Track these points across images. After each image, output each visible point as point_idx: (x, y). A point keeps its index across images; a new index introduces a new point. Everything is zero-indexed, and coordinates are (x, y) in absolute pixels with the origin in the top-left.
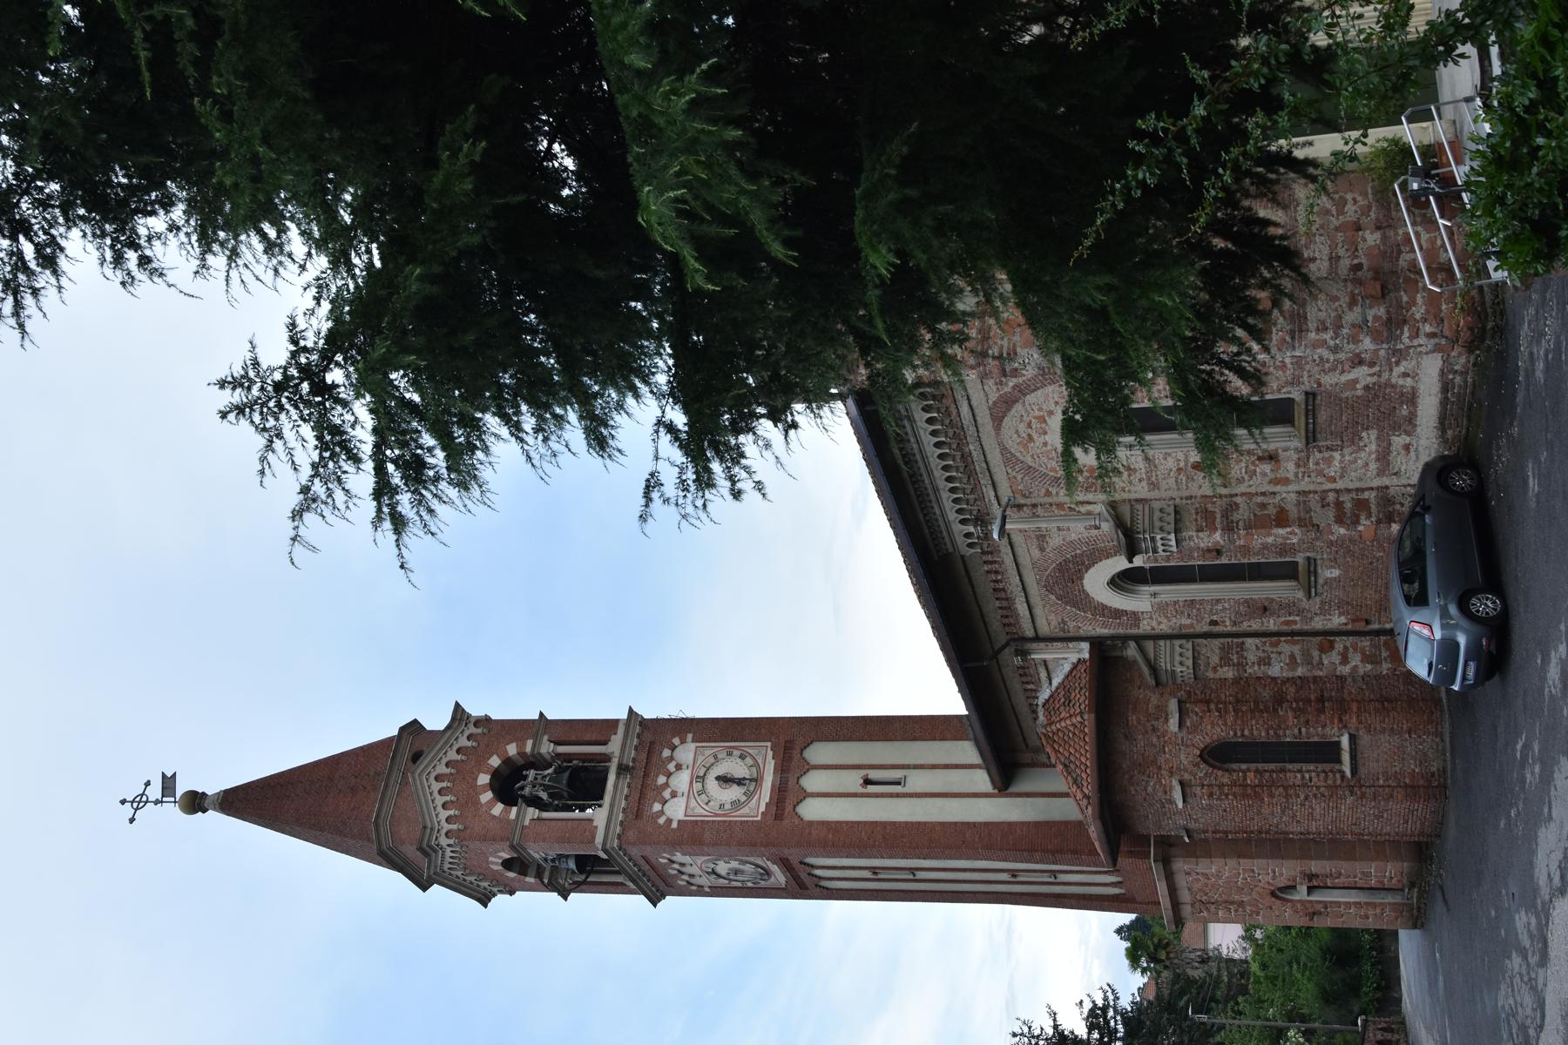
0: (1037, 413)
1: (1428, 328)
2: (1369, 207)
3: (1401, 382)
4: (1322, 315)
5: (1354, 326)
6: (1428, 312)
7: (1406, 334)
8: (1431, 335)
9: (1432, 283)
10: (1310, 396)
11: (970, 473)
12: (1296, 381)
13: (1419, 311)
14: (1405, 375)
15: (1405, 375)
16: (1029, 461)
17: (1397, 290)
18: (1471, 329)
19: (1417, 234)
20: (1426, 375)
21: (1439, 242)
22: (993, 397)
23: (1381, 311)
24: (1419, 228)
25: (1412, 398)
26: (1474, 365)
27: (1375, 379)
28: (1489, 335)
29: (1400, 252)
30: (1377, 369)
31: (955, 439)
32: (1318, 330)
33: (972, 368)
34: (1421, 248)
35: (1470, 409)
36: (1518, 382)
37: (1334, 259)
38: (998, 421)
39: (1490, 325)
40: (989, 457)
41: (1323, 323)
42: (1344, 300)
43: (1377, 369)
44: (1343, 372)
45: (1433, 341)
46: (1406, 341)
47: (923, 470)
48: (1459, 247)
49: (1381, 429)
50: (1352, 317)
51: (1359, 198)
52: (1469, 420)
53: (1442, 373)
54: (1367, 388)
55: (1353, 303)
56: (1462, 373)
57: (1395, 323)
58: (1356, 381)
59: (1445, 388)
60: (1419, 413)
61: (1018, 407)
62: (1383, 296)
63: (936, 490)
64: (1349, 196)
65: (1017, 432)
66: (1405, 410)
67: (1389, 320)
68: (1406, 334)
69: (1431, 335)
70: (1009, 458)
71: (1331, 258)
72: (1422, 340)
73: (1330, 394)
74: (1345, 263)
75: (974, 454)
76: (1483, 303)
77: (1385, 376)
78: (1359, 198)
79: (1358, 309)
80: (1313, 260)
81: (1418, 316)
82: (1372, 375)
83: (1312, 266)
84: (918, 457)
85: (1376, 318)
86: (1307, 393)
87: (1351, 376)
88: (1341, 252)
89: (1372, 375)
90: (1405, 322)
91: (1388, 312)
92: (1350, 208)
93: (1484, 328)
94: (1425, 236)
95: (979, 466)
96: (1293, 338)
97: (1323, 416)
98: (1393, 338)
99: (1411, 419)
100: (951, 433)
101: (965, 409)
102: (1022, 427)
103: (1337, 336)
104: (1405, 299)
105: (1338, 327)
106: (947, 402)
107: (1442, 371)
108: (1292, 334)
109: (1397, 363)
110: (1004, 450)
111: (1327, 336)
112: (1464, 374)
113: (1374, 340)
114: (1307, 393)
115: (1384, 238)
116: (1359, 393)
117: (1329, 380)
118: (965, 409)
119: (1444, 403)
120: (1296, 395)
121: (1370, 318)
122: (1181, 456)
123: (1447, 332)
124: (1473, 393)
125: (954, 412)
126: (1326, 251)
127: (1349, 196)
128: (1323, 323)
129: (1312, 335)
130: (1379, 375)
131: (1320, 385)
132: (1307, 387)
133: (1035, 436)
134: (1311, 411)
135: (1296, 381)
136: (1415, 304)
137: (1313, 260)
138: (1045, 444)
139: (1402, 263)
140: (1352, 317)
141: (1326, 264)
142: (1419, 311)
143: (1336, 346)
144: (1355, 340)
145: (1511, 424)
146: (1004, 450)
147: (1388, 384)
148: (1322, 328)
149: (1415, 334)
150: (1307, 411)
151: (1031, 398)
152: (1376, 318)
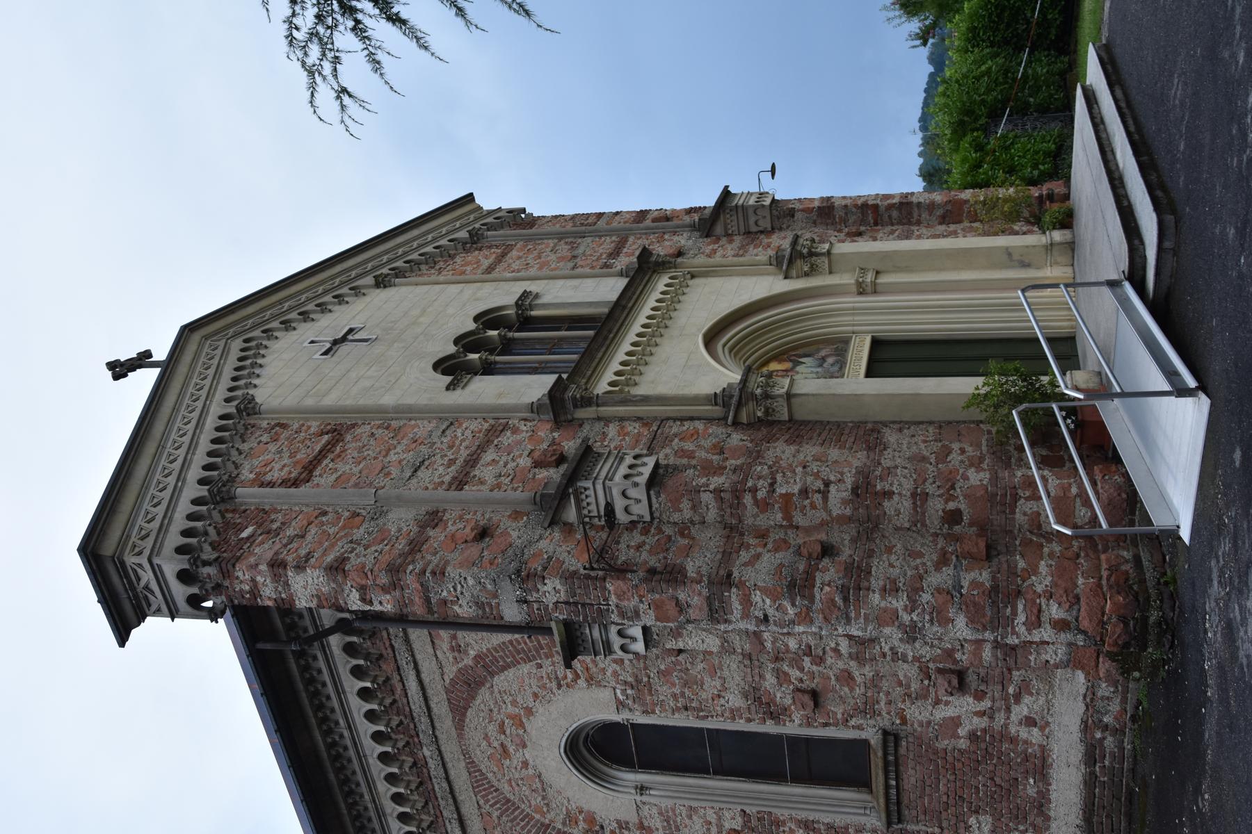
0: (511, 709)
1: (1055, 611)
2: (981, 459)
3: (1024, 733)
4: (896, 572)
5: (939, 590)
6: (1054, 584)
7: (1021, 618)
8: (1060, 625)
9: (1058, 522)
10: (890, 737)
11: (430, 798)
12: (867, 709)
13: (1042, 580)
14: (1030, 722)
15: (1030, 722)
16: (506, 788)
17: (1010, 551)
18: (1123, 620)
19: (1043, 478)
20: (1062, 716)
21: (1074, 490)
22: (451, 671)
23: (985, 577)
24: (1046, 473)
25: (1040, 766)
26: (1134, 718)
27: (982, 723)
28: (1152, 638)
29: (1016, 498)
30: (986, 704)
31: (401, 733)
32: (884, 590)
33: (385, 590)
34: (1048, 495)
35: (1130, 801)
36: (1206, 701)
37: (920, 498)
38: (459, 712)
39: (1154, 616)
40: (452, 773)
41: (894, 582)
42: (930, 557)
43: (986, 704)
44: (937, 702)
45: (1066, 637)
46: (1022, 629)
47: (360, 777)
48: (1104, 496)
49: (997, 818)
50: (936, 579)
51: (969, 449)
52: (1129, 816)
53: (1086, 728)
54: (973, 736)
55: (943, 561)
56: (1115, 732)
57: (996, 604)
58: (956, 722)
59: (1092, 755)
60: (1053, 796)
61: (483, 695)
62: (989, 557)
63: (381, 814)
64: (956, 446)
65: (486, 737)
66: (1030, 788)
67: (995, 589)
68: (1021, 618)
69: (1060, 625)
70: (480, 782)
71: (914, 495)
72: (1046, 633)
73: (919, 741)
74: (936, 507)
75: (432, 764)
76: (1143, 581)
77: (1000, 718)
78: (969, 449)
79: (948, 571)
80: (889, 494)
81: (1039, 589)
82: (981, 714)
83: (886, 504)
84: (352, 752)
85: (974, 584)
86: (885, 733)
87: (949, 712)
88: (930, 489)
89: (981, 714)
90: (1019, 593)
91: (994, 578)
92: (955, 458)
93: (1145, 619)
94: (1053, 482)
95: (440, 787)
96: (846, 599)
97: (911, 777)
98: (1001, 622)
99: (1042, 804)
100: (395, 721)
101: (412, 685)
102: (492, 729)
103: (913, 606)
104: (1021, 564)
105: (915, 590)
106: (388, 667)
107: (1084, 722)
108: (844, 591)
109: (1018, 698)
110: (471, 765)
111: (899, 603)
112: (1118, 732)
113: (971, 621)
114: (885, 733)
115: (995, 479)
116: (963, 744)
117: (917, 713)
118: (412, 685)
119: (1090, 782)
120: (871, 734)
121: (965, 584)
122: (712, 817)
123: (1085, 624)
124: (1133, 771)
125: (399, 687)
126: (908, 485)
127: (956, 446)
128: (894, 582)
129: (875, 598)
130: (989, 714)
131: (904, 721)
132: (885, 721)
133: (511, 749)
134: (893, 767)
135: (867, 709)
136: (1035, 571)
137: (889, 494)
138: (525, 764)
139: (1018, 516)
140: (936, 579)
141: (907, 504)
142: (1042, 580)
143: (913, 625)
144: (945, 621)
145: (1198, 791)
146: (471, 765)
147: (1004, 736)
148: (891, 589)
149: (1035, 622)
150: (886, 764)
151: (500, 681)
152: (974, 584)
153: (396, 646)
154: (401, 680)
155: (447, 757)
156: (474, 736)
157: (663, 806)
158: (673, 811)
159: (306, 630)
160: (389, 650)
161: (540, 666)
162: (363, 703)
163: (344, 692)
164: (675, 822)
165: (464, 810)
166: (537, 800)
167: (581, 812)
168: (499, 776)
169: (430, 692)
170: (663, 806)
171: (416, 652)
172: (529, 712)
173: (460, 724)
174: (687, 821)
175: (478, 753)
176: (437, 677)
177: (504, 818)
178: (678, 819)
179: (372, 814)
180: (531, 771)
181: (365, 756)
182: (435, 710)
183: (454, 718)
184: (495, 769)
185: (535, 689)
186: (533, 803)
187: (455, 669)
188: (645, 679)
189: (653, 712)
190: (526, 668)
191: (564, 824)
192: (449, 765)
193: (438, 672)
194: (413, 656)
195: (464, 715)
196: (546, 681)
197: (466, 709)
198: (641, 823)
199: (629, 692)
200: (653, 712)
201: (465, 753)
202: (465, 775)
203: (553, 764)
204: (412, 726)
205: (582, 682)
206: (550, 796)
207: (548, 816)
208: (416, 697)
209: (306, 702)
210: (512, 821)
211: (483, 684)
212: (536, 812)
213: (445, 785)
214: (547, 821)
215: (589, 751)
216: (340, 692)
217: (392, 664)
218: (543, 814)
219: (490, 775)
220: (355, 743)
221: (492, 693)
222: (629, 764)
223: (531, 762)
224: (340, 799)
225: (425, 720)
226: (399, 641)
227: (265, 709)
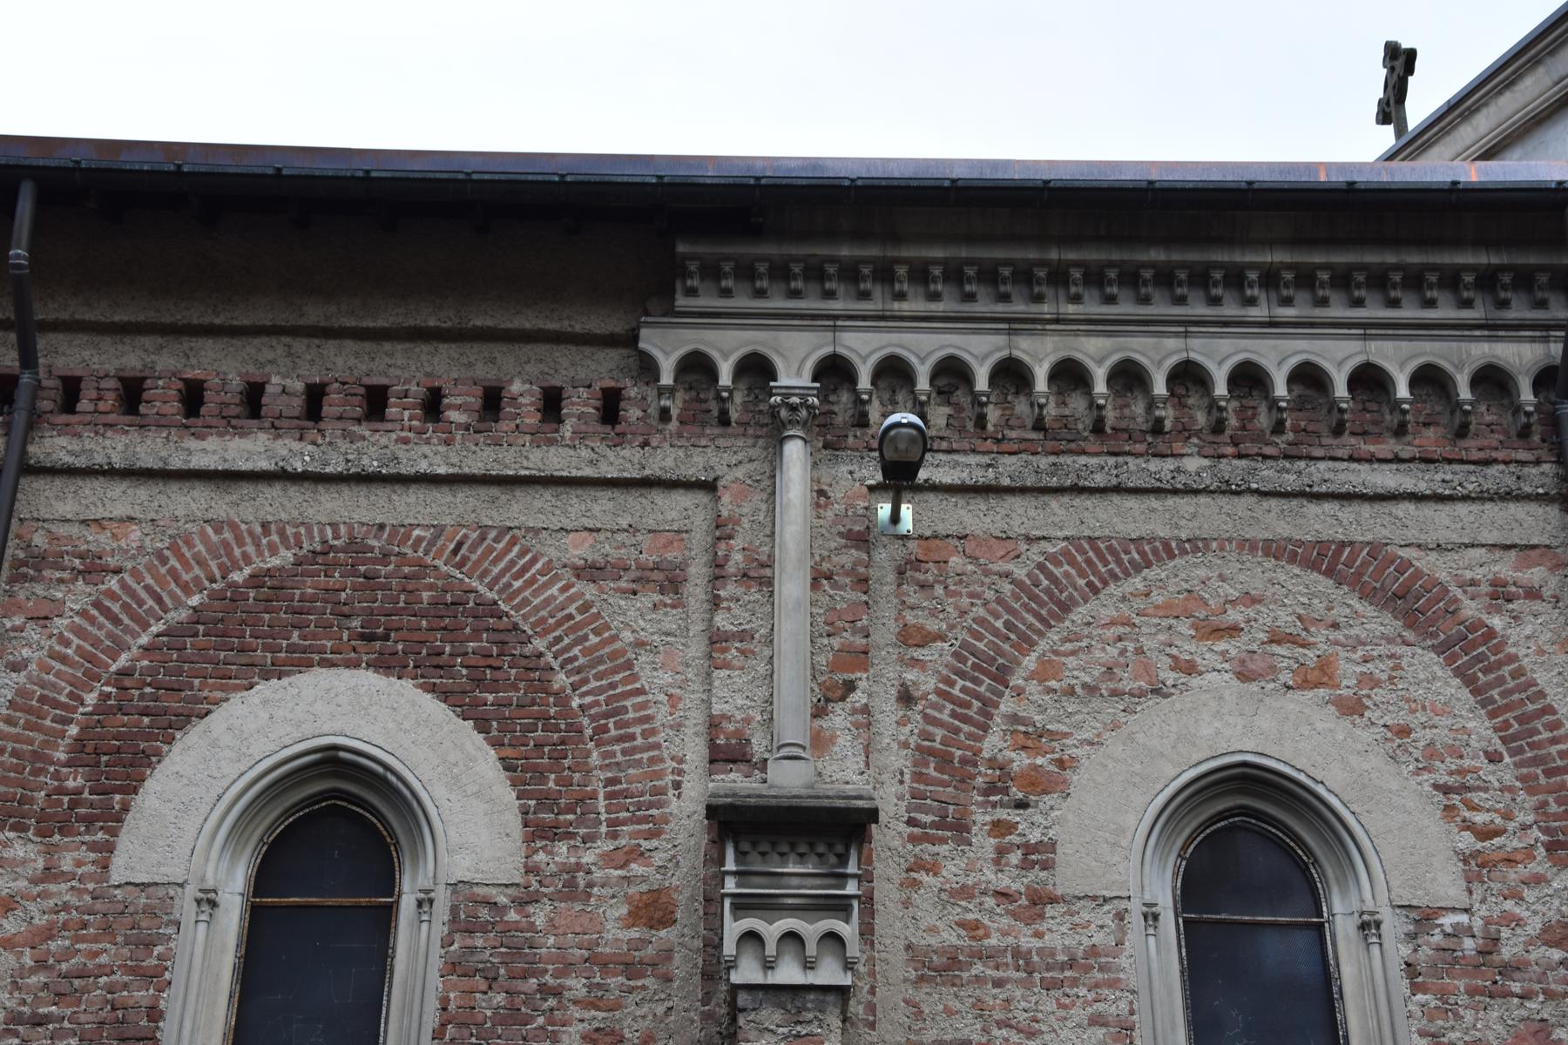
70: (1108, 561)
101: (1385, 478)
118: (1385, 478)
153: (1493, 470)
154: (1397, 460)
155: (1184, 504)
156: (1256, 575)
157: (1123, 961)
158: (1113, 984)
159: (691, 292)
160: (1476, 455)
161: (1494, 758)
162: (734, 358)
163: (1365, 337)
164: (1075, 982)
165: (1017, 503)
166: (1077, 671)
167: (1061, 764)
168: (1139, 603)
169: (1366, 510)
170: (1123, 961)
171: (1475, 507)
172: (1352, 708)
173: (1276, 550)
174: (1079, 1014)
175: (1202, 572)
176: (1412, 534)
177: (1007, 588)
178: (1082, 992)
179: (1019, 307)
180: (1170, 677)
181: (1186, 335)
182: (1312, 509)
183: (1300, 543)
184: (1158, 598)
185: (1422, 736)
186: (1071, 662)
187: (1442, 576)
188: (1516, 987)
189: (1416, 988)
190: (1481, 730)
191: (1014, 718)
192: (1153, 502)
193: (1430, 539)
194: (1466, 498)
195: (1314, 566)
196: (1452, 763)
197: (1329, 573)
198: (1053, 900)
199: (1469, 944)
200: (1416, 988)
201: (1196, 545)
202: (1142, 530)
203: (1206, 731)
204: (1268, 450)
205: (1467, 841)
206: (1096, 703)
207: (1033, 687)
208: (1342, 477)
209: (1372, 258)
210: (999, 601)
211: (1409, 626)
212: (1041, 660)
213: (1099, 480)
214: (1016, 680)
215: (1220, 816)
216: (1096, 325)
217: (1439, 451)
218: (1039, 676)
219: (1137, 583)
220: (1226, 324)
221: (1390, 641)
222: (264, 879)
223: (1195, 681)
224: (1483, 259)
225: (1290, 481)
226: (1510, 481)
227: (1216, 177)
